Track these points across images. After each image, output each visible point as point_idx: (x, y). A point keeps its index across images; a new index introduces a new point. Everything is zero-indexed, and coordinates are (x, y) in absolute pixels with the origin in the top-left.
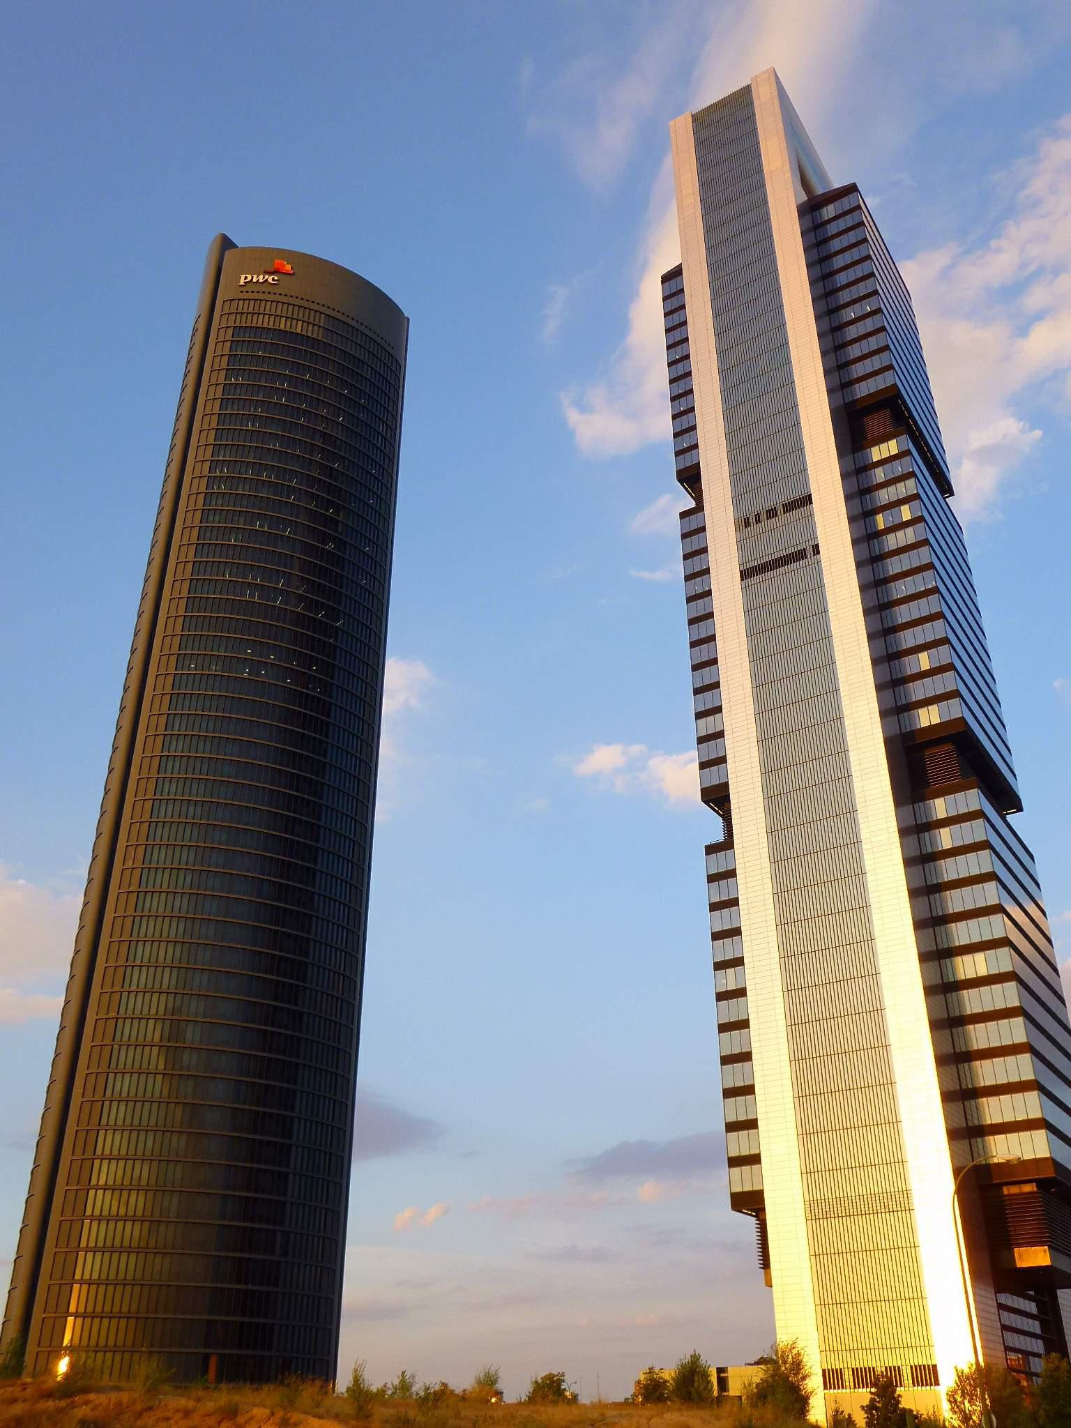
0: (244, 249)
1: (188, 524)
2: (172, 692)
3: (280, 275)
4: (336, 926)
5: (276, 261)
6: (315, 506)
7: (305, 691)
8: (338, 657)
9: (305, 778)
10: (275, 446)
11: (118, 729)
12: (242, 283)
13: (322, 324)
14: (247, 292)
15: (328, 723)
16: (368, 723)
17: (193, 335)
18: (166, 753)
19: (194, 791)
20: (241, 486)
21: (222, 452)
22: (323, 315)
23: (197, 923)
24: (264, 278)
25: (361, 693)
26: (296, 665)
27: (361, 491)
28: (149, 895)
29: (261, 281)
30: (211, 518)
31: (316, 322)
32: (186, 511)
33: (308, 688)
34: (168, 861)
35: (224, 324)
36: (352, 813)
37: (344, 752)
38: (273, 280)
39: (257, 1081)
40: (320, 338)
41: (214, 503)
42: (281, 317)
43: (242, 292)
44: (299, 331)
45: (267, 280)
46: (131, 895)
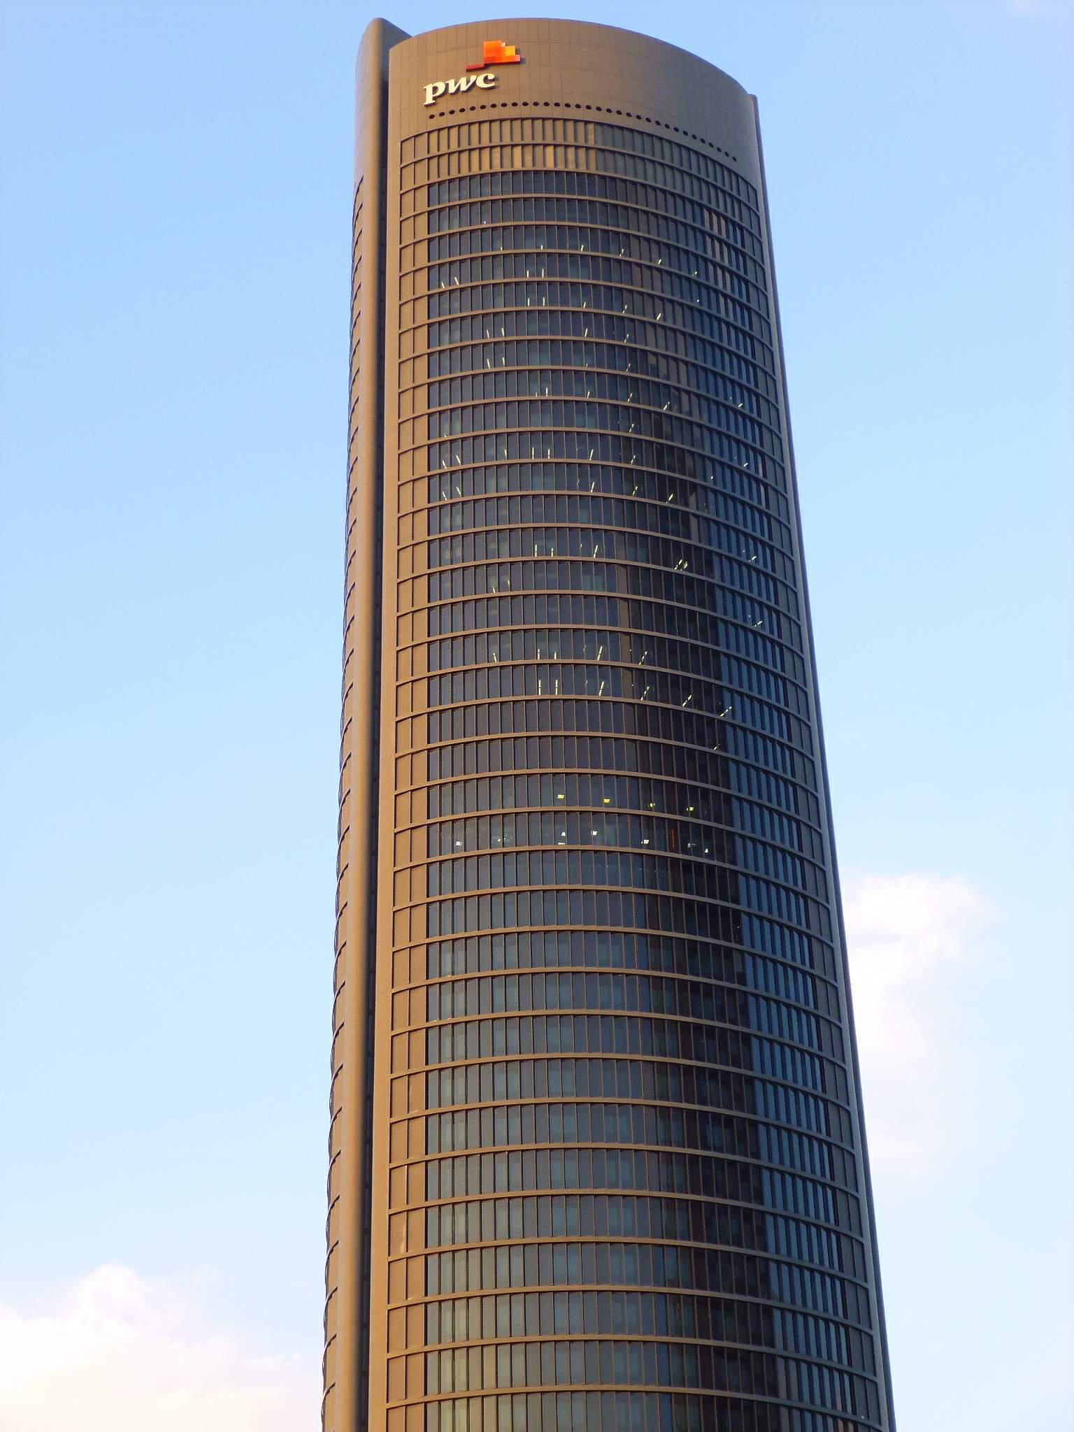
0: (424, 37)
1: (406, 677)
2: (429, 381)
4: (830, 1421)
5: (485, 43)
6: (638, 494)
7: (680, 856)
8: (725, 670)
9: (713, 1073)
10: (543, 393)
11: (335, 1116)
12: (429, 100)
13: (591, 143)
14: (442, 114)
15: (717, 654)
16: (827, 1020)
17: (356, 217)
18: (435, 1022)
19: (500, 1087)
20: (492, 483)
21: (446, 427)
22: (591, 127)
23: (548, 1348)
24: (468, 82)
25: (823, 1174)
26: (656, 809)
28: (447, 1211)
29: (464, 87)
31: (581, 142)
32: (401, 249)
33: (685, 851)
34: (474, 1140)
35: (409, 185)
36: (836, 1313)
38: (486, 80)
39: (684, 1105)
40: (593, 170)
41: (447, 198)
42: (513, 146)
43: (432, 117)
44: (550, 165)
45: (474, 83)
46: (412, 1263)
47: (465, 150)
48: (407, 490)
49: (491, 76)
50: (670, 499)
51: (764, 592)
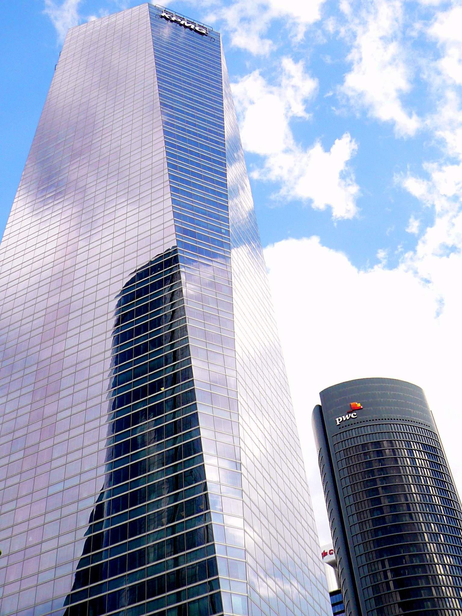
3: (357, 411)
12: (338, 423)
24: (349, 416)
27: (427, 448)
29: (348, 418)
30: (373, 568)
37: (445, 610)
38: (354, 415)
47: (365, 565)
48: (347, 499)
49: (355, 414)
50: (427, 540)
51: (439, 484)
